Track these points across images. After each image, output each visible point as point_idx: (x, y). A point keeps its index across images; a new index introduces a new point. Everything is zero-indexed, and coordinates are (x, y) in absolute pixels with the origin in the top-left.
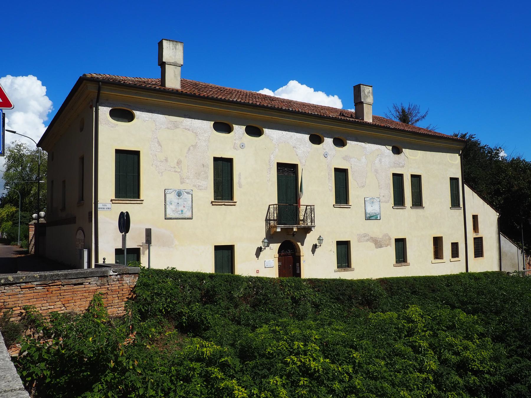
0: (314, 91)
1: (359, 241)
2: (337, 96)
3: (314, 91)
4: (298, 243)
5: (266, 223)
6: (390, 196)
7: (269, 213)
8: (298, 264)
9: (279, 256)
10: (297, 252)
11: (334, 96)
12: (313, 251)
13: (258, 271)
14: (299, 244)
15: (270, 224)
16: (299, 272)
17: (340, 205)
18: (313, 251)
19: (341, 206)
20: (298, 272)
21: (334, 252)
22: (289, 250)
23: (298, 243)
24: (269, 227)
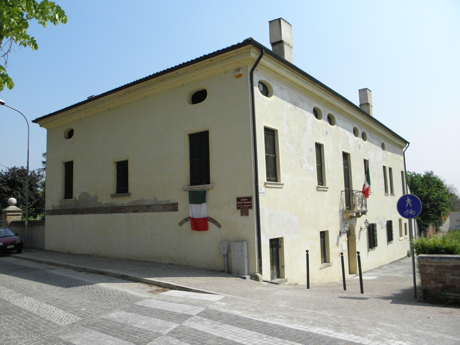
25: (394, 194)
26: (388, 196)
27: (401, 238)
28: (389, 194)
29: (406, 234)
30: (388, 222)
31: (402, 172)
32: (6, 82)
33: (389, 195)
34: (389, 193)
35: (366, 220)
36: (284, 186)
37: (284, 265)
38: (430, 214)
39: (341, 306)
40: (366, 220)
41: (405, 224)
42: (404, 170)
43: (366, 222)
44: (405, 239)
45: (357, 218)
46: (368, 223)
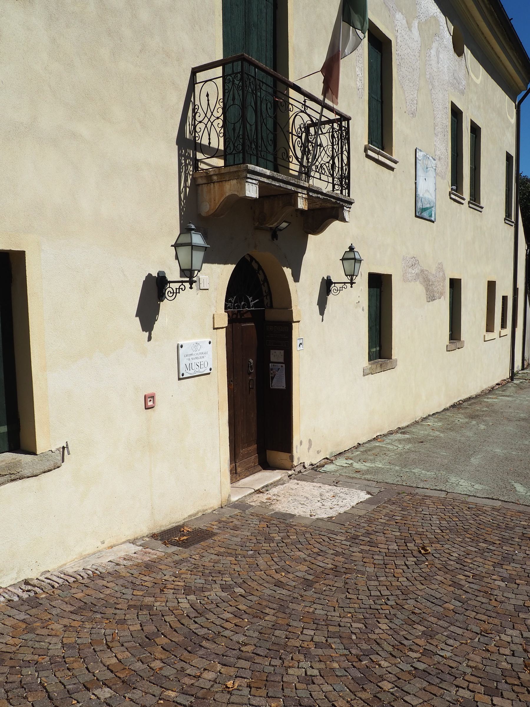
0: (150, 275)
1: (405, 280)
2: (153, 275)
3: (150, 275)
4: (285, 269)
5: (180, 155)
6: (448, 164)
7: (195, 113)
8: (276, 355)
9: (230, 321)
10: (271, 307)
11: (136, 316)
12: (322, 304)
13: (153, 397)
14: (288, 272)
15: (196, 168)
16: (283, 385)
17: (378, 153)
18: (322, 304)
19: (381, 159)
20: (278, 384)
21: (363, 310)
22: (250, 299)
23: (285, 269)
24: (194, 179)
25: (482, 208)
26: (463, 204)
27: (490, 336)
28: (464, 199)
29: (503, 325)
30: (298, 281)
31: (509, 157)
32: (340, 117)
33: (466, 202)
34: (464, 196)
35: (351, 249)
36: (483, 210)
37: (369, 287)
38: (42, 595)
39: (180, 564)
40: (351, 249)
41: (505, 299)
42: (513, 153)
43: (351, 255)
44: (500, 337)
45: (310, 236)
46: (355, 259)
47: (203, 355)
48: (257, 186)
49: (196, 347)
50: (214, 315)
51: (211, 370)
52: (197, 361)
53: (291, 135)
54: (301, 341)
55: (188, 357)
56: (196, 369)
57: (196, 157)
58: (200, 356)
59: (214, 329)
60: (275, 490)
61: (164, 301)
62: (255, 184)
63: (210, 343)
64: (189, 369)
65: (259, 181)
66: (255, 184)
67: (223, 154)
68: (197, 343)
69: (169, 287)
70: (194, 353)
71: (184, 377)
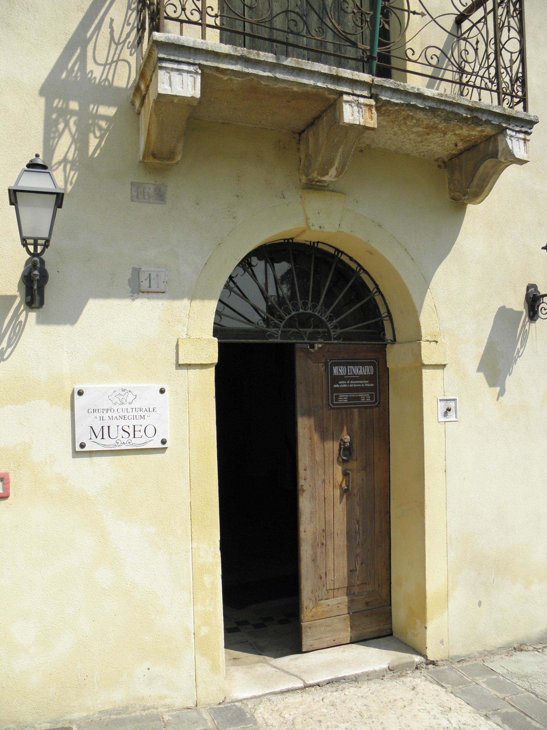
10: (394, 341)
47: (142, 414)
48: (199, 78)
49: (121, 397)
50: (178, 339)
51: (164, 442)
52: (122, 423)
53: (406, 13)
54: (134, 410)
55: (98, 415)
56: (120, 437)
57: (464, 74)
58: (132, 414)
59: (179, 366)
60: (447, 613)
61: (538, 321)
62: (188, 72)
63: (162, 391)
64: (100, 436)
65: (200, 65)
66: (188, 72)
67: (465, 69)
68: (123, 390)
69: (543, 302)
70: (115, 408)
71: (85, 449)
